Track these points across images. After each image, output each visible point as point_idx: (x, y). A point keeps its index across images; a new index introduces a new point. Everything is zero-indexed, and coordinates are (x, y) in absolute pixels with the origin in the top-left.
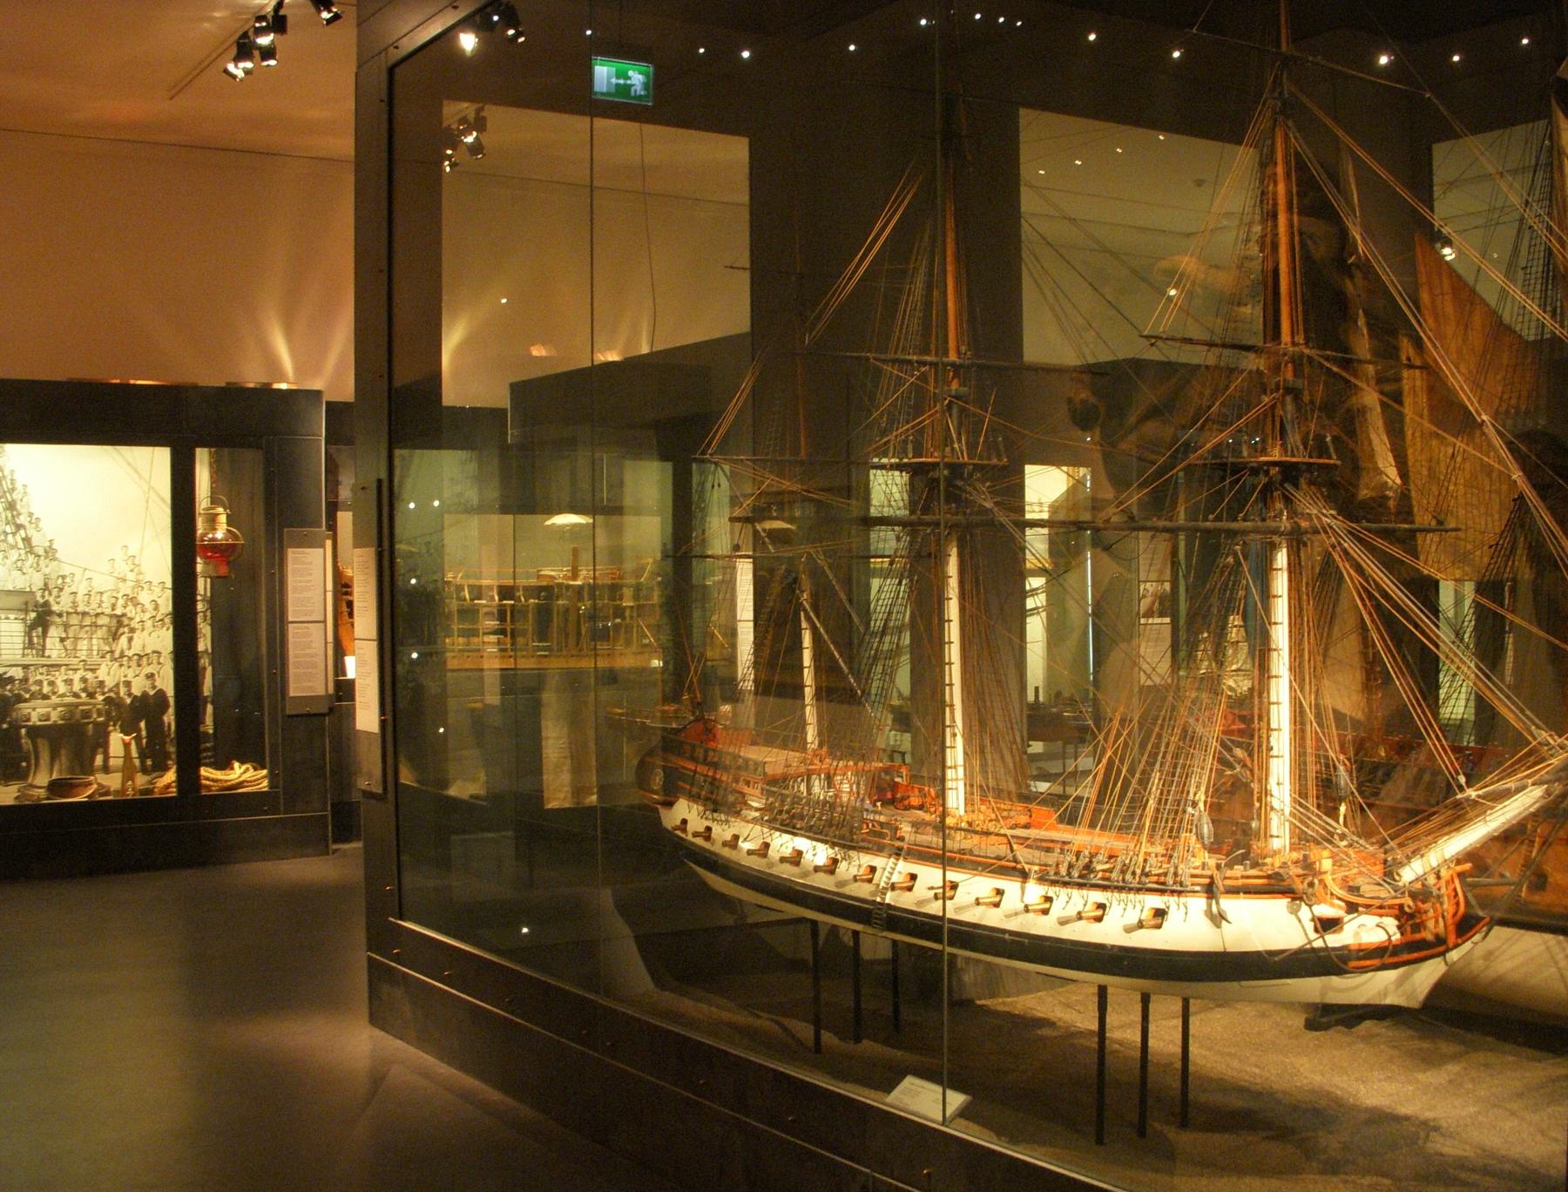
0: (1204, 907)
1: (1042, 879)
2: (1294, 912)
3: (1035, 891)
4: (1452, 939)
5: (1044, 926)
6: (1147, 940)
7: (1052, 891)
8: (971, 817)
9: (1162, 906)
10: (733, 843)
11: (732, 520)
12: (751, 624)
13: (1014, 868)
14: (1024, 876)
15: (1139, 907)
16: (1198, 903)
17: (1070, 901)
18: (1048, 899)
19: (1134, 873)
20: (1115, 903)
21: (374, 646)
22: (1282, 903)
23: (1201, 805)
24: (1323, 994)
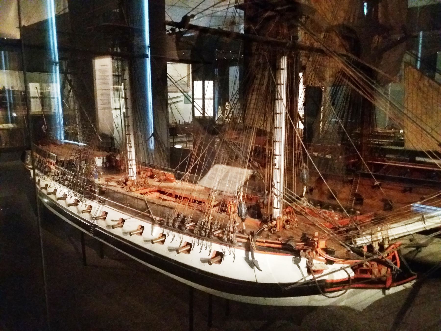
0: (244, 255)
1: (161, 225)
2: (297, 262)
3: (158, 230)
4: (389, 282)
5: (160, 249)
6: (215, 269)
7: (166, 232)
8: (139, 180)
9: (221, 251)
10: (46, 187)
11: (113, 75)
12: (299, 104)
13: (149, 216)
14: (153, 222)
15: (208, 249)
16: (241, 252)
17: (175, 239)
18: (164, 235)
19: (205, 231)
20: (196, 244)
21: (212, 101)
22: (290, 258)
23: (241, 198)
24: (309, 302)
